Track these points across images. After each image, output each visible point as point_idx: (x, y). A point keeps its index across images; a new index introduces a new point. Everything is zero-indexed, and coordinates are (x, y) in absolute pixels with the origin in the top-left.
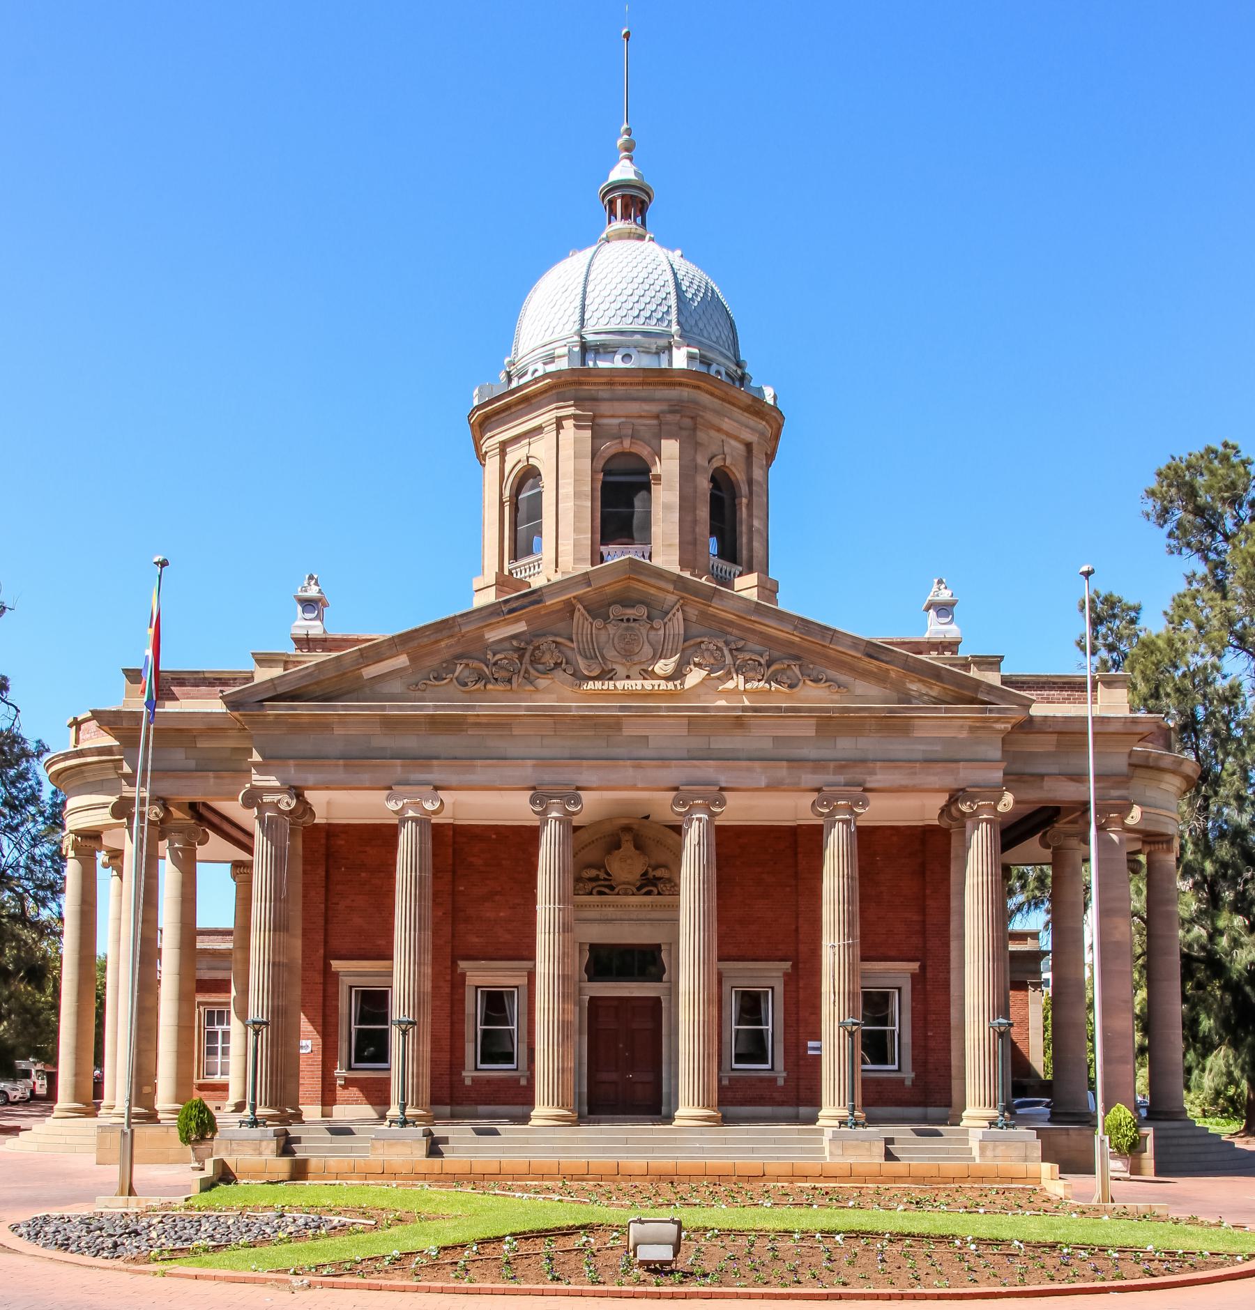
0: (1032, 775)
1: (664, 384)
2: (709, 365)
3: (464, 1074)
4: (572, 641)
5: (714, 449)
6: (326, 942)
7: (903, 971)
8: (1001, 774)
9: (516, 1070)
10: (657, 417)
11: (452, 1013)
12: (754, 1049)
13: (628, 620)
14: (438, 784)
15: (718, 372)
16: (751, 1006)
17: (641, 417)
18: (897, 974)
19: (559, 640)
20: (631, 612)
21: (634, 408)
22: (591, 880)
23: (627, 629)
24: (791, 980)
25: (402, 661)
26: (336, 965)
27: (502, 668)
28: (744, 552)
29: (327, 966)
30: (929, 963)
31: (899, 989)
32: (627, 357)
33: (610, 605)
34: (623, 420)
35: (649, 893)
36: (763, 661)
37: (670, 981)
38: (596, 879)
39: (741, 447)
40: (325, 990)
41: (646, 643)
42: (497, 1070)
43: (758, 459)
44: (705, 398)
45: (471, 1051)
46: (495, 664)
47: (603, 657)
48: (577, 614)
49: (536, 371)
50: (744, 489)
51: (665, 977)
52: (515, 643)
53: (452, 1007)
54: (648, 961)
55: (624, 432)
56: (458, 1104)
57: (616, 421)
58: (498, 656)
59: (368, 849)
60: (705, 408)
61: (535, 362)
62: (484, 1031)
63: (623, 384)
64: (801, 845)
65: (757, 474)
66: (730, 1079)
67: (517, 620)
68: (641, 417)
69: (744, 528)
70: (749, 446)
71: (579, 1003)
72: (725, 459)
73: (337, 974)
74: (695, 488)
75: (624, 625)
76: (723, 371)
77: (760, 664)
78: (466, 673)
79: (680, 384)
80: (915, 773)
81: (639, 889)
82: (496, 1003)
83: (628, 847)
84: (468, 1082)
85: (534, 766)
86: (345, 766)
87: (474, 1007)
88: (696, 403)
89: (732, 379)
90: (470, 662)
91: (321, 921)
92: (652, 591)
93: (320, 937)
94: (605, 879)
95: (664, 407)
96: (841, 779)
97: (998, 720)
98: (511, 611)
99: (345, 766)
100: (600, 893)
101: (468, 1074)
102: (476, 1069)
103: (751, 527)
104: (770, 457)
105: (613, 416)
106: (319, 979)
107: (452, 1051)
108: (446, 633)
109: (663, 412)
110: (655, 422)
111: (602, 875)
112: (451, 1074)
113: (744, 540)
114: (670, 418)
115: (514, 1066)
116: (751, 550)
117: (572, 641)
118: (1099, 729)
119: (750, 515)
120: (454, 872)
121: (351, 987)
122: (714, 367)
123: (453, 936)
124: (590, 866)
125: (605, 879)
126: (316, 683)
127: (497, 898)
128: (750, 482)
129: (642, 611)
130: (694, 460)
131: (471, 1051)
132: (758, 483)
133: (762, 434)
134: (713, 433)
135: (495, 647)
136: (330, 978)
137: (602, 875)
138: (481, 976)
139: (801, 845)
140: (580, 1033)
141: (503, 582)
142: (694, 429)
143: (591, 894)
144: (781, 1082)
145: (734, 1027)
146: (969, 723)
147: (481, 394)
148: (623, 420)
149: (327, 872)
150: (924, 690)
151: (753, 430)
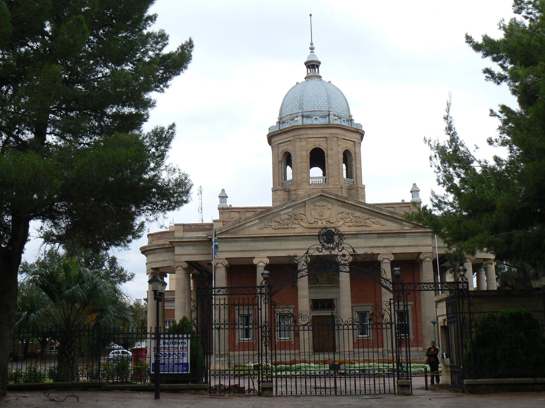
35: (329, 283)
54: (329, 304)
56: (146, 331)
69: (354, 168)
113: (354, 171)
116: (356, 174)
119: (356, 164)
128: (355, 153)
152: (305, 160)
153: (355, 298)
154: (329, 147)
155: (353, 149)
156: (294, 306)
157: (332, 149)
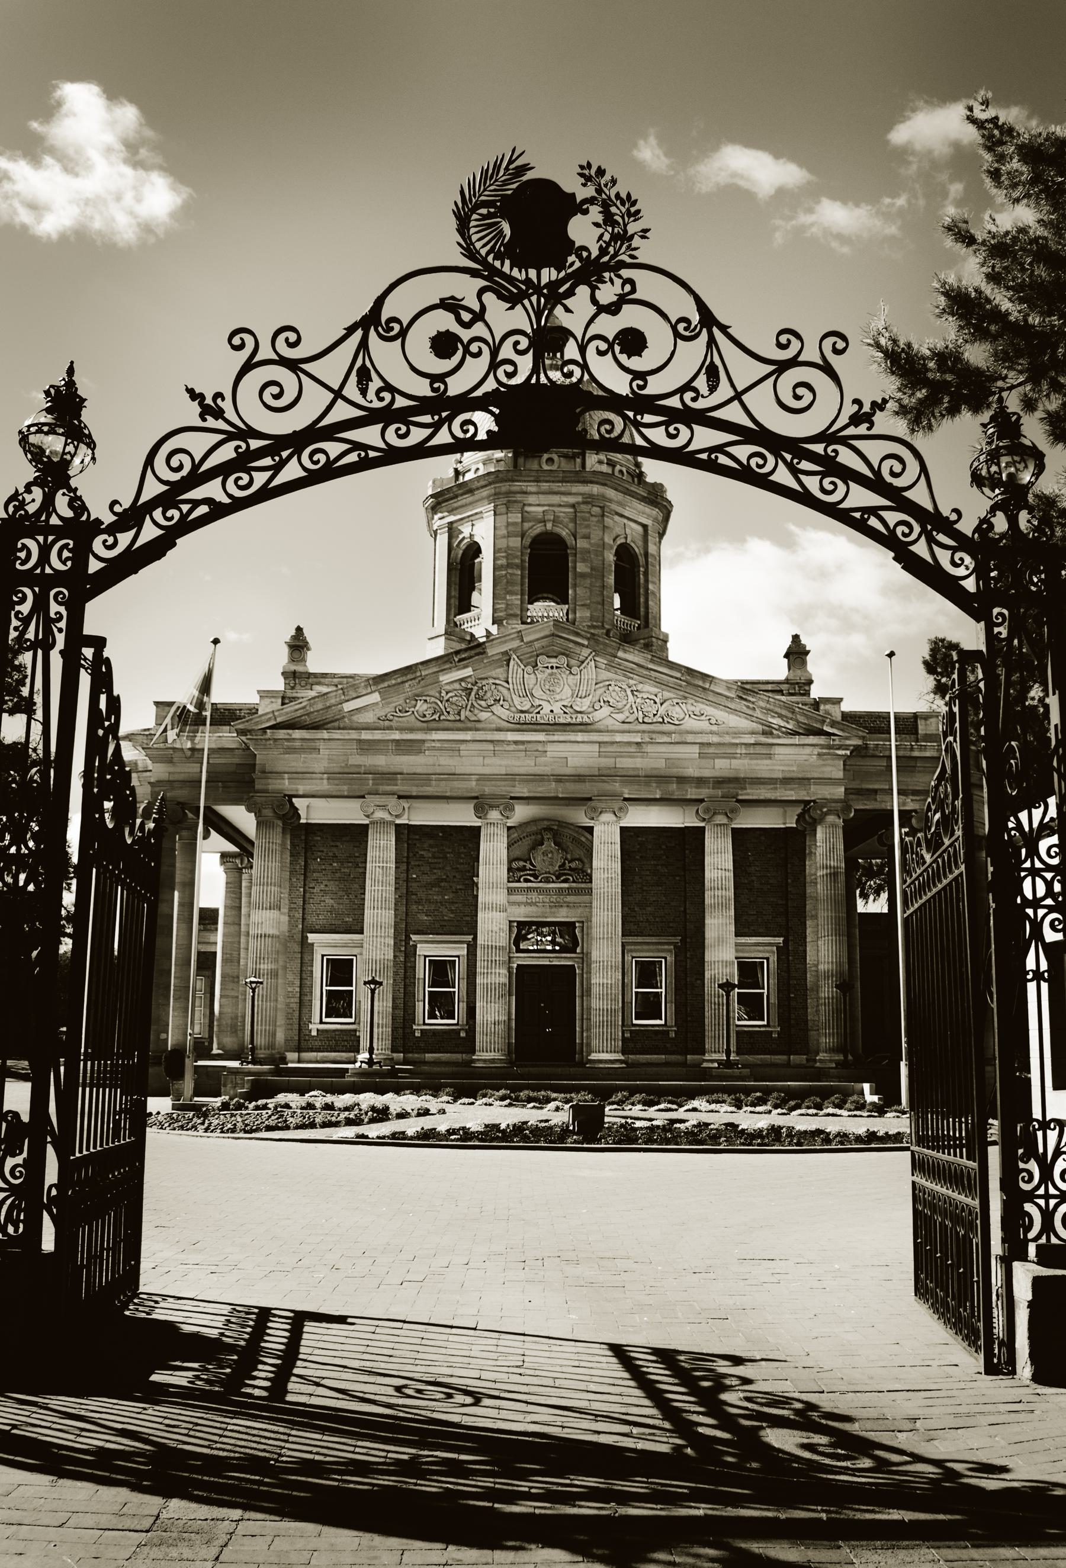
0: (868, 790)
1: (579, 482)
2: (614, 466)
3: (311, 1026)
4: (508, 682)
5: (618, 530)
6: (304, 919)
7: (770, 945)
8: (842, 789)
9: (457, 1024)
10: (573, 506)
11: (405, 978)
12: (649, 1007)
13: (552, 667)
14: (401, 794)
15: (621, 472)
16: (647, 973)
17: (560, 506)
18: (764, 949)
19: (497, 682)
20: (553, 661)
21: (556, 499)
22: (519, 869)
23: (551, 674)
24: (680, 952)
25: (376, 697)
26: (312, 937)
27: (452, 703)
28: (642, 609)
29: (304, 938)
30: (791, 938)
31: (768, 959)
32: (16, 629)
33: (538, 656)
34: (546, 508)
35: (566, 881)
36: (657, 700)
37: (582, 953)
38: (524, 869)
39: (640, 529)
40: (302, 958)
41: (566, 686)
42: (336, 1023)
43: (652, 538)
44: (611, 493)
45: (421, 1008)
46: (448, 700)
47: (532, 695)
48: (512, 663)
49: (478, 469)
50: (642, 560)
51: (578, 950)
52: (463, 684)
53: (405, 972)
54: (570, 936)
55: (546, 518)
57: (541, 509)
58: (450, 694)
59: (338, 844)
60: (610, 501)
61: (477, 463)
62: (329, 992)
63: (547, 482)
64: (687, 845)
65: (652, 549)
66: (631, 1032)
67: (466, 667)
68: (560, 506)
69: (642, 591)
70: (645, 527)
71: (510, 969)
72: (626, 538)
73: (312, 944)
74: (604, 560)
75: (549, 671)
76: (624, 470)
77: (655, 703)
78: (425, 706)
79: (592, 482)
80: (776, 789)
81: (558, 877)
82: (440, 970)
83: (549, 845)
84: (314, 1033)
85: (478, 780)
86: (328, 779)
87: (422, 971)
88: (603, 497)
89: (633, 477)
90: (428, 698)
91: (300, 902)
92: (571, 645)
93: (299, 915)
94: (530, 870)
95: (580, 499)
96: (720, 793)
97: (840, 747)
98: (460, 660)
99: (328, 779)
100: (527, 881)
101: (314, 1028)
102: (321, 1022)
103: (647, 589)
104: (661, 535)
105: (538, 505)
106: (297, 949)
107: (405, 1010)
108: (410, 676)
109: (578, 503)
110: (572, 510)
111: (528, 866)
112: (404, 1028)
113: (642, 600)
114: (583, 507)
115: (455, 1022)
117: (508, 682)
118: (901, 753)
119: (647, 581)
120: (408, 863)
121: (323, 956)
122: (618, 467)
123: (407, 915)
124: (518, 859)
125: (530, 870)
126: (307, 714)
127: (442, 884)
128: (646, 555)
129: (563, 660)
130: (603, 539)
131: (421, 1008)
132: (653, 555)
133: (655, 520)
134: (616, 518)
135: (448, 688)
136: (306, 948)
137: (528, 866)
138: (428, 949)
139: (687, 845)
140: (510, 995)
141: (452, 630)
142: (603, 516)
143: (519, 881)
144: (672, 1035)
145: (634, 990)
146: (816, 751)
147: (434, 487)
148: (546, 508)
149: (306, 862)
150: (783, 724)
151: (649, 516)
152: (518, 561)
153: (632, 925)
154: (581, 531)
155: (640, 543)
156: (470, 938)
157: (587, 537)
